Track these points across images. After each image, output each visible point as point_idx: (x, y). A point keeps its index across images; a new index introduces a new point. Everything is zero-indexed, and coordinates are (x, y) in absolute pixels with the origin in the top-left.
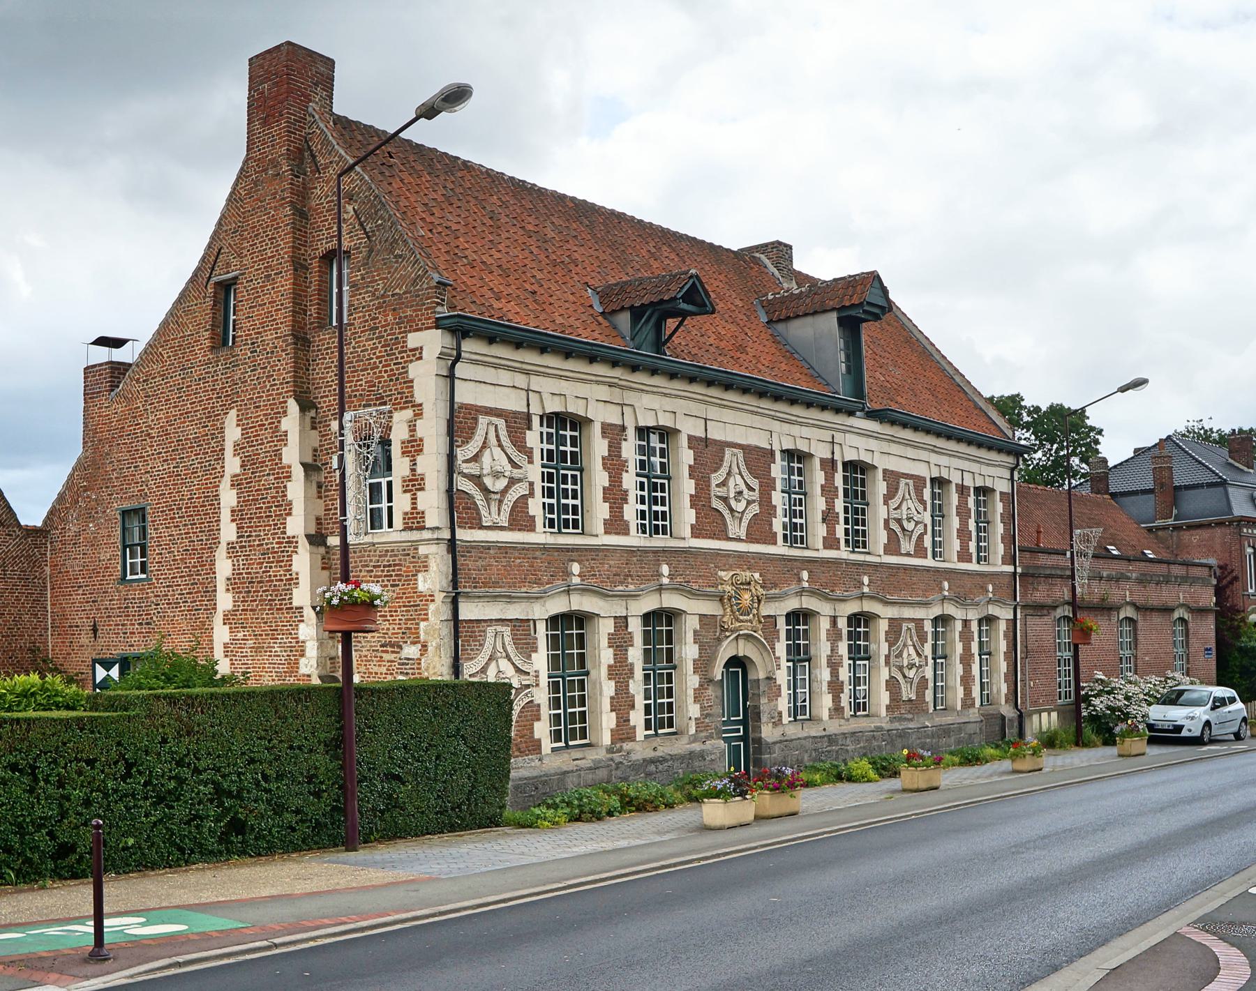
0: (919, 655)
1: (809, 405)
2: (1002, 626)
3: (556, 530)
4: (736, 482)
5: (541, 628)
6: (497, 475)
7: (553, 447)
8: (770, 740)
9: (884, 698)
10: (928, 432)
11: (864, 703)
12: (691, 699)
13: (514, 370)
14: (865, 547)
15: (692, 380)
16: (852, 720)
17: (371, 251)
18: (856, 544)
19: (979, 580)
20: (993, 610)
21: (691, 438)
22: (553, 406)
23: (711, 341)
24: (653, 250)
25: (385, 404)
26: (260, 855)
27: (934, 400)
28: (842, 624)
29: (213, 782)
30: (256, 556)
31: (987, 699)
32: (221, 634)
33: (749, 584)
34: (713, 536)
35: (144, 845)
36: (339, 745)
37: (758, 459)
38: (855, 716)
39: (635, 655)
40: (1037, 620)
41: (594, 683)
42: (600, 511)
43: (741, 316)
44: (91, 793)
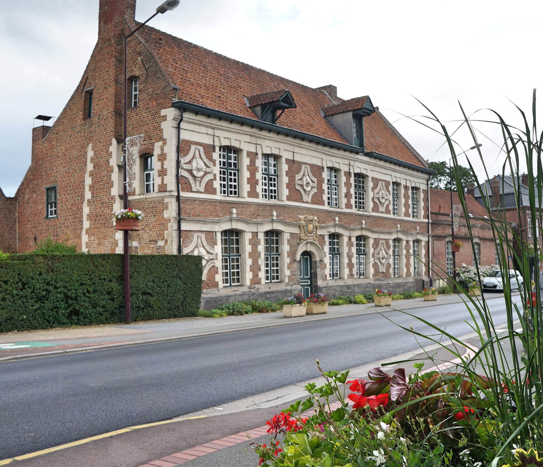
0: (387, 254)
1: (339, 149)
2: (423, 244)
3: (226, 195)
4: (307, 179)
5: (219, 235)
6: (199, 170)
7: (225, 160)
8: (321, 286)
9: (372, 271)
10: (391, 163)
11: (363, 273)
12: (286, 268)
13: (208, 127)
14: (363, 208)
15: (287, 135)
16: (358, 279)
17: (147, 76)
18: (360, 207)
19: (413, 224)
20: (419, 237)
21: (287, 160)
22: (225, 143)
23: (298, 121)
24: (276, 85)
25: (151, 139)
26: (86, 325)
27: (403, 156)
28: (354, 240)
29: (64, 293)
30: (99, 205)
31: (419, 274)
32: (85, 238)
33: (312, 221)
34: (296, 201)
35: (31, 319)
36: (122, 279)
37: (317, 170)
38: (359, 278)
39: (261, 248)
40: (438, 242)
41: (243, 260)
42: (246, 188)
43: (313, 113)
44: (6, 295)
